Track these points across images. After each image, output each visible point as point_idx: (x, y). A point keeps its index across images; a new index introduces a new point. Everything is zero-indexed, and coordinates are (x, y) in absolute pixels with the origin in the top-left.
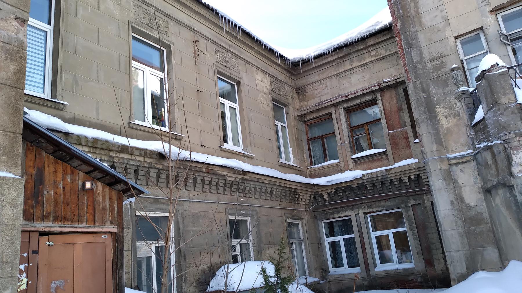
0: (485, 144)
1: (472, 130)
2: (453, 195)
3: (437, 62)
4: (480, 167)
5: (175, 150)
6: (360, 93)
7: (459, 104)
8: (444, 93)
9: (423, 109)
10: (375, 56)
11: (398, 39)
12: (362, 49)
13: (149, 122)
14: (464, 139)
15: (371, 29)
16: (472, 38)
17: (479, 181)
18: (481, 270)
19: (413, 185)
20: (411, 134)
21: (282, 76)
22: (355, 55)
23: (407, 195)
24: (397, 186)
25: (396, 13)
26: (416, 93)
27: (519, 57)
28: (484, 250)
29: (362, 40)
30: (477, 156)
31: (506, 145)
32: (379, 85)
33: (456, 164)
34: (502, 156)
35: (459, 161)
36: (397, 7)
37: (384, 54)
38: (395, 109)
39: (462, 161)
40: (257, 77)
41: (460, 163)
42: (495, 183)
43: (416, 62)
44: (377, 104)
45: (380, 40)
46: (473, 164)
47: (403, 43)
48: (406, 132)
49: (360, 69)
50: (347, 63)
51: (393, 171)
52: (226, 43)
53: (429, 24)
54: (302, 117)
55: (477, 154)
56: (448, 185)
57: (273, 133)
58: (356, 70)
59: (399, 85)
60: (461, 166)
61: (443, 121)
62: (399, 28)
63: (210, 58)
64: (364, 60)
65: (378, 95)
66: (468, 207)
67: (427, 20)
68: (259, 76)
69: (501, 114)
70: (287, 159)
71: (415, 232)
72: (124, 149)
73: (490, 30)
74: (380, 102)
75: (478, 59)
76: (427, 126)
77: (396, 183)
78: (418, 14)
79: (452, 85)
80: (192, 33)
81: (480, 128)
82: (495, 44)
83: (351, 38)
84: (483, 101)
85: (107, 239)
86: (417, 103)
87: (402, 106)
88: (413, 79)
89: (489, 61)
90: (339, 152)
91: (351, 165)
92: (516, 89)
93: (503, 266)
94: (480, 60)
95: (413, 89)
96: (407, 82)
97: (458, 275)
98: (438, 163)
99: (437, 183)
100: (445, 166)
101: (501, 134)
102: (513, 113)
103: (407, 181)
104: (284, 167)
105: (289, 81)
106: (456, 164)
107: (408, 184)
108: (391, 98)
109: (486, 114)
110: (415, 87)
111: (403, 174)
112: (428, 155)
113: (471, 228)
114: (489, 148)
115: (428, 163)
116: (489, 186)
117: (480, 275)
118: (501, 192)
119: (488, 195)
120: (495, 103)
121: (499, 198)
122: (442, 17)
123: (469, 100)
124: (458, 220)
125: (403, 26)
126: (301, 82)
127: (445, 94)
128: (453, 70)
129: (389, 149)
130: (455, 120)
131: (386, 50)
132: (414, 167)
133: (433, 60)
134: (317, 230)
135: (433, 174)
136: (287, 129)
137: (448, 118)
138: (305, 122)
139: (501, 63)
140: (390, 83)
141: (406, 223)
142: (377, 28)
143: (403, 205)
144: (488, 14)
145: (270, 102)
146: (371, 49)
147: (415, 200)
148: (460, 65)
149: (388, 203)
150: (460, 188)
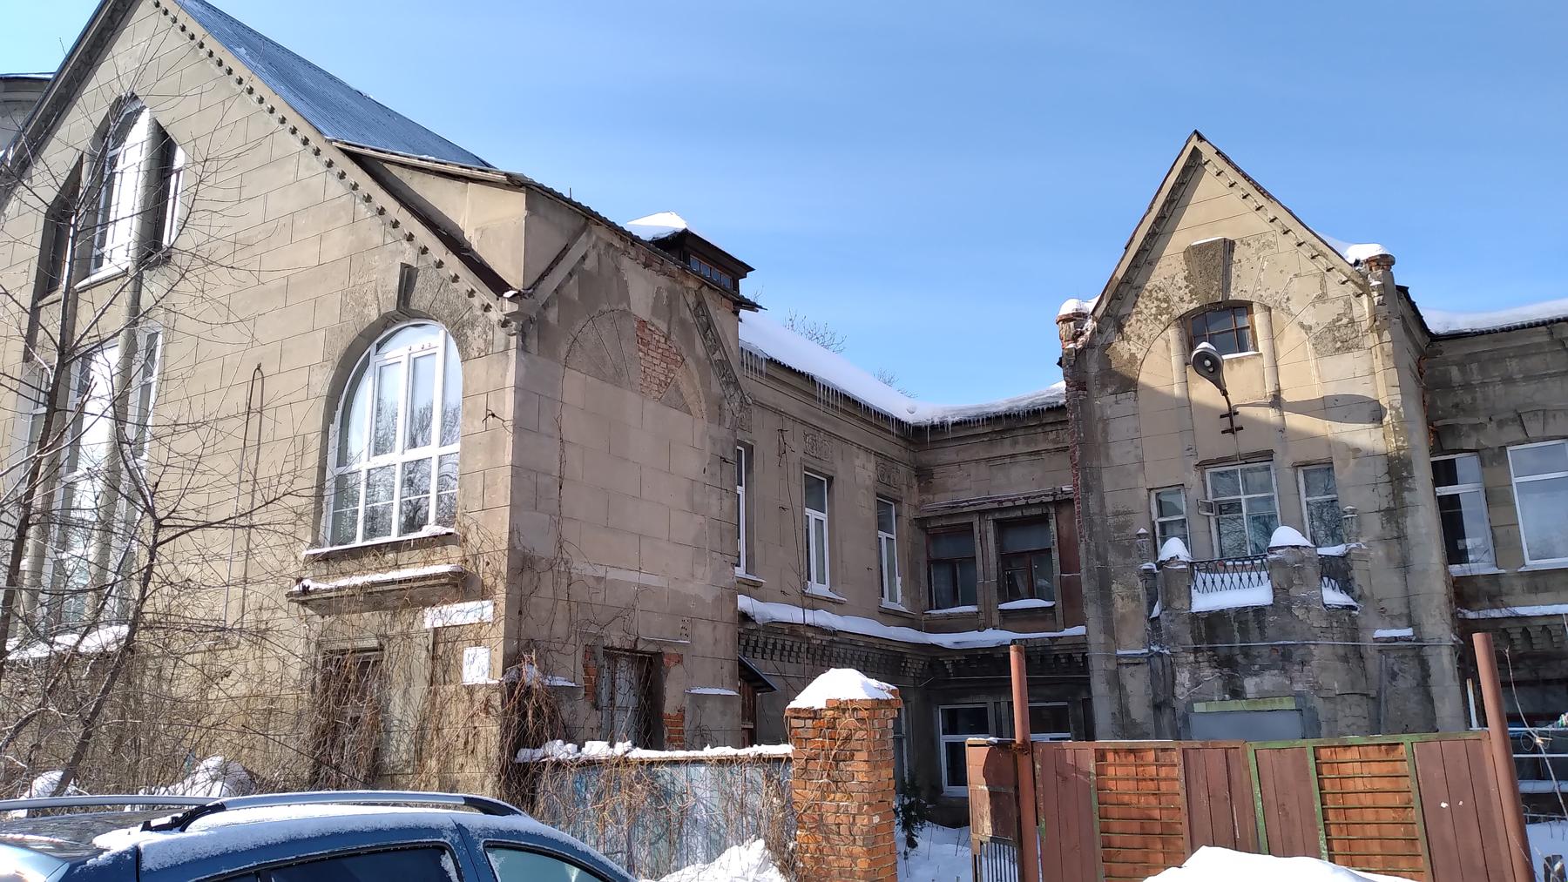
3: (1121, 518)
6: (1023, 502)
10: (1054, 441)
21: (894, 449)
22: (1021, 432)
32: (1054, 495)
33: (1127, 665)
39: (1134, 661)
40: (857, 462)
46: (1147, 668)
50: (1007, 442)
52: (819, 418)
54: (921, 523)
58: (1020, 458)
60: (1132, 668)
61: (1119, 603)
65: (1052, 510)
70: (893, 598)
80: (777, 417)
89: (1174, 548)
90: (980, 594)
91: (996, 621)
92: (1194, 592)
100: (1112, 666)
104: (889, 616)
105: (906, 455)
106: (1127, 665)
126: (926, 458)
133: (1117, 514)
134: (931, 722)
136: (893, 544)
138: (925, 529)
146: (1048, 428)
149: (1047, 691)
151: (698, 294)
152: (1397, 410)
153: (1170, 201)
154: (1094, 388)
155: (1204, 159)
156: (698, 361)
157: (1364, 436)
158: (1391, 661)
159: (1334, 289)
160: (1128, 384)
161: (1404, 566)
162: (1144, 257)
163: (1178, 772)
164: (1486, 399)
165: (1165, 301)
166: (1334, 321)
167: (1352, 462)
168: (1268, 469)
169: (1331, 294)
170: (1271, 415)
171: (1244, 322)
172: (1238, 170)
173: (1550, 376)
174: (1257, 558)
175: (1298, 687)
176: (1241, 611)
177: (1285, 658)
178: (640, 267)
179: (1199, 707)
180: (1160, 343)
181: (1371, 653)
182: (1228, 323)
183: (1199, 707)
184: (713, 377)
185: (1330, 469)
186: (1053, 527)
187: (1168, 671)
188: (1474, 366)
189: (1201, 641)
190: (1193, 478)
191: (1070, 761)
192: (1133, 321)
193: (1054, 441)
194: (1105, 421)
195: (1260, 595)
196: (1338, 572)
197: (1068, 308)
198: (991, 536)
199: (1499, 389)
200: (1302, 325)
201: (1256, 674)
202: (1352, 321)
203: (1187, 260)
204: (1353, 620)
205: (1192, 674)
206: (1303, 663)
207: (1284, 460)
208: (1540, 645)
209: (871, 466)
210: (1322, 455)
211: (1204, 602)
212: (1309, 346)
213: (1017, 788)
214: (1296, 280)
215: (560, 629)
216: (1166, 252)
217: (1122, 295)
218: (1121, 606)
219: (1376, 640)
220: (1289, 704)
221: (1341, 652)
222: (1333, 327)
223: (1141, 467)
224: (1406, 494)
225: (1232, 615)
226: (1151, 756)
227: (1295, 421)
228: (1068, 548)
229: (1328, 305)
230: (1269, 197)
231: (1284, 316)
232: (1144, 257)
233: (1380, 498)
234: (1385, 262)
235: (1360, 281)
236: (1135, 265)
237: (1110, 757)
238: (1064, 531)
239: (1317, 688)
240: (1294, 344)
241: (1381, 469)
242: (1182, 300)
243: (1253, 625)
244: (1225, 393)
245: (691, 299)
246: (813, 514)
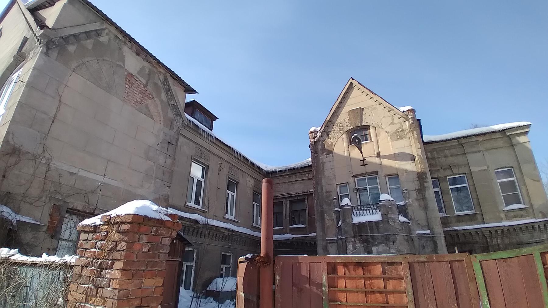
3: (328, 194)
5: (204, 219)
13: (192, 204)
39: (332, 242)
40: (247, 179)
46: (336, 244)
52: (235, 163)
57: (251, 209)
60: (331, 244)
61: (327, 222)
63: (226, 170)
67: (327, 173)
68: (249, 179)
72: (181, 218)
85: (177, 263)
89: (346, 201)
91: (288, 232)
100: (324, 243)
110: (317, 204)
129: (308, 226)
133: (326, 192)
145: (252, 192)
151: (165, 76)
153: (344, 98)
154: (320, 153)
156: (162, 101)
157: (408, 166)
158: (423, 242)
159: (396, 120)
160: (331, 152)
161: (426, 208)
162: (335, 114)
163: (406, 285)
164: (439, 162)
168: (376, 178)
169: (395, 122)
170: (377, 160)
171: (367, 132)
172: (364, 87)
174: (376, 203)
176: (370, 223)
177: (387, 240)
178: (134, 54)
181: (416, 239)
182: (363, 133)
184: (169, 110)
185: (398, 177)
186: (306, 202)
187: (344, 244)
188: (435, 152)
190: (351, 180)
191: (304, 272)
194: (323, 163)
195: (377, 217)
196: (403, 210)
197: (312, 129)
198: (288, 205)
199: (443, 159)
204: (409, 227)
207: (382, 174)
208: (462, 239)
209: (252, 181)
210: (395, 172)
211: (357, 219)
213: (258, 297)
215: (35, 191)
217: (329, 125)
218: (328, 223)
219: (417, 234)
221: (406, 238)
222: (396, 132)
223: (335, 176)
226: (378, 270)
227: (385, 162)
228: (311, 208)
229: (395, 125)
231: (380, 129)
232: (335, 114)
233: (415, 185)
234: (413, 111)
235: (405, 117)
237: (341, 270)
238: (310, 203)
240: (383, 136)
241: (415, 176)
243: (375, 228)
244: (362, 153)
245: (162, 77)
246: (230, 193)
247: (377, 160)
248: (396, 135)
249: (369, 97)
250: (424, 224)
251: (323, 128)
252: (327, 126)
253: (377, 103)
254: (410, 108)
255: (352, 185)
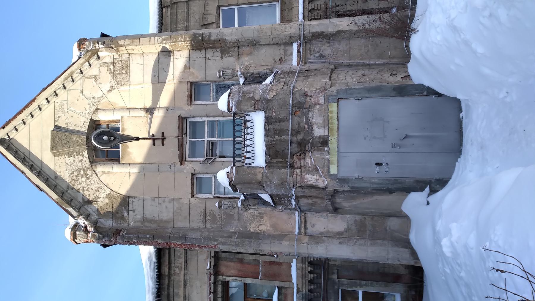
0: (293, 200)
1: (278, 206)
2: (334, 240)
3: (208, 218)
4: (312, 210)
6: (212, 296)
7: (252, 211)
8: (238, 220)
9: (247, 243)
10: (180, 270)
11: (172, 246)
12: (169, 282)
14: (284, 216)
15: (152, 266)
16: (198, 184)
17: (325, 214)
18: (408, 236)
19: (318, 271)
20: (267, 259)
22: (172, 290)
23: (327, 279)
24: (316, 287)
25: (148, 240)
26: (230, 245)
27: (228, 155)
28: (390, 229)
29: (160, 278)
30: (302, 209)
31: (298, 185)
32: (210, 274)
33: (306, 228)
34: (306, 190)
35: (303, 225)
36: (143, 238)
37: (182, 260)
38: (239, 265)
39: (304, 223)
41: (305, 225)
42: (329, 202)
43: (201, 236)
44: (228, 282)
45: (167, 261)
46: (309, 214)
47: (178, 243)
48: (265, 262)
49: (187, 288)
51: (300, 287)
53: (171, 215)
55: (300, 209)
56: (323, 242)
59: (217, 257)
60: (308, 225)
61: (263, 228)
62: (163, 242)
64: (181, 281)
65: (220, 278)
66: (347, 230)
67: (166, 215)
69: (270, 182)
71: (364, 283)
73: (197, 169)
74: (227, 279)
75: (218, 185)
76: (264, 243)
77: (312, 287)
78: (158, 221)
79: (233, 211)
81: (278, 201)
82: (211, 168)
83: (153, 289)
84: (255, 192)
86: (240, 246)
87: (238, 259)
88: (216, 243)
89: (222, 176)
92: (253, 165)
93: (406, 217)
94: (220, 183)
95: (225, 246)
96: (217, 250)
97: (412, 258)
98: (302, 244)
99: (319, 251)
100: (306, 239)
101: (288, 187)
102: (272, 173)
103: (312, 275)
106: (306, 228)
107: (316, 275)
108: (227, 266)
109: (267, 193)
110: (224, 244)
111: (305, 277)
112: (291, 251)
113: (368, 234)
114: (297, 199)
115: (299, 253)
116: (331, 208)
117: (413, 238)
118: (338, 200)
119: (340, 211)
120: (260, 183)
121: (343, 202)
122: (170, 202)
123: (251, 201)
124: (358, 242)
125: (162, 238)
127: (239, 219)
128: (220, 207)
129: (277, 283)
130: (265, 218)
131: (180, 257)
132: (300, 265)
133: (205, 221)
135: (311, 252)
137: (262, 223)
139: (228, 169)
140: (212, 264)
141: (354, 289)
142: (154, 259)
143: (336, 287)
144: (182, 167)
146: (172, 272)
147: (333, 273)
148: (218, 200)
150: (328, 232)
152: (163, 40)
155: (6, 137)
159: (93, 71)
160: (125, 201)
165: (80, 171)
166: (111, 73)
167: (191, 70)
169: (96, 73)
170: (158, 115)
172: (15, 117)
173: (188, 10)
174: (238, 122)
175: (322, 100)
177: (301, 107)
179: (334, 170)
180: (103, 178)
183: (334, 170)
187: (308, 192)
189: (286, 162)
190: (189, 167)
192: (86, 193)
193: (180, 270)
194: (145, 220)
195: (258, 120)
197: (68, 233)
200: (109, 91)
201: (311, 127)
202: (113, 63)
203: (60, 155)
205: (309, 172)
206: (306, 96)
207: (185, 110)
210: (186, 88)
211: (260, 158)
212: (122, 88)
214: (84, 92)
216: (52, 167)
217: (69, 197)
218: (265, 227)
219: (298, 64)
220: (334, 107)
222: (113, 74)
223: (174, 201)
224: (212, 38)
225: (269, 139)
227: (165, 100)
229: (101, 76)
230: (33, 101)
231: (104, 101)
232: (51, 180)
233: (214, 56)
234: (81, 42)
235: (89, 54)
236: (54, 188)
239: (324, 89)
240: (115, 98)
241: (198, 54)
242: (81, 161)
243: (277, 126)
244: (137, 139)
247: (158, 115)
248: (119, 76)
249: (37, 113)
250: (282, 52)
251: (71, 210)
252: (70, 203)
253: (52, 99)
254: (75, 46)
255: (198, 168)
